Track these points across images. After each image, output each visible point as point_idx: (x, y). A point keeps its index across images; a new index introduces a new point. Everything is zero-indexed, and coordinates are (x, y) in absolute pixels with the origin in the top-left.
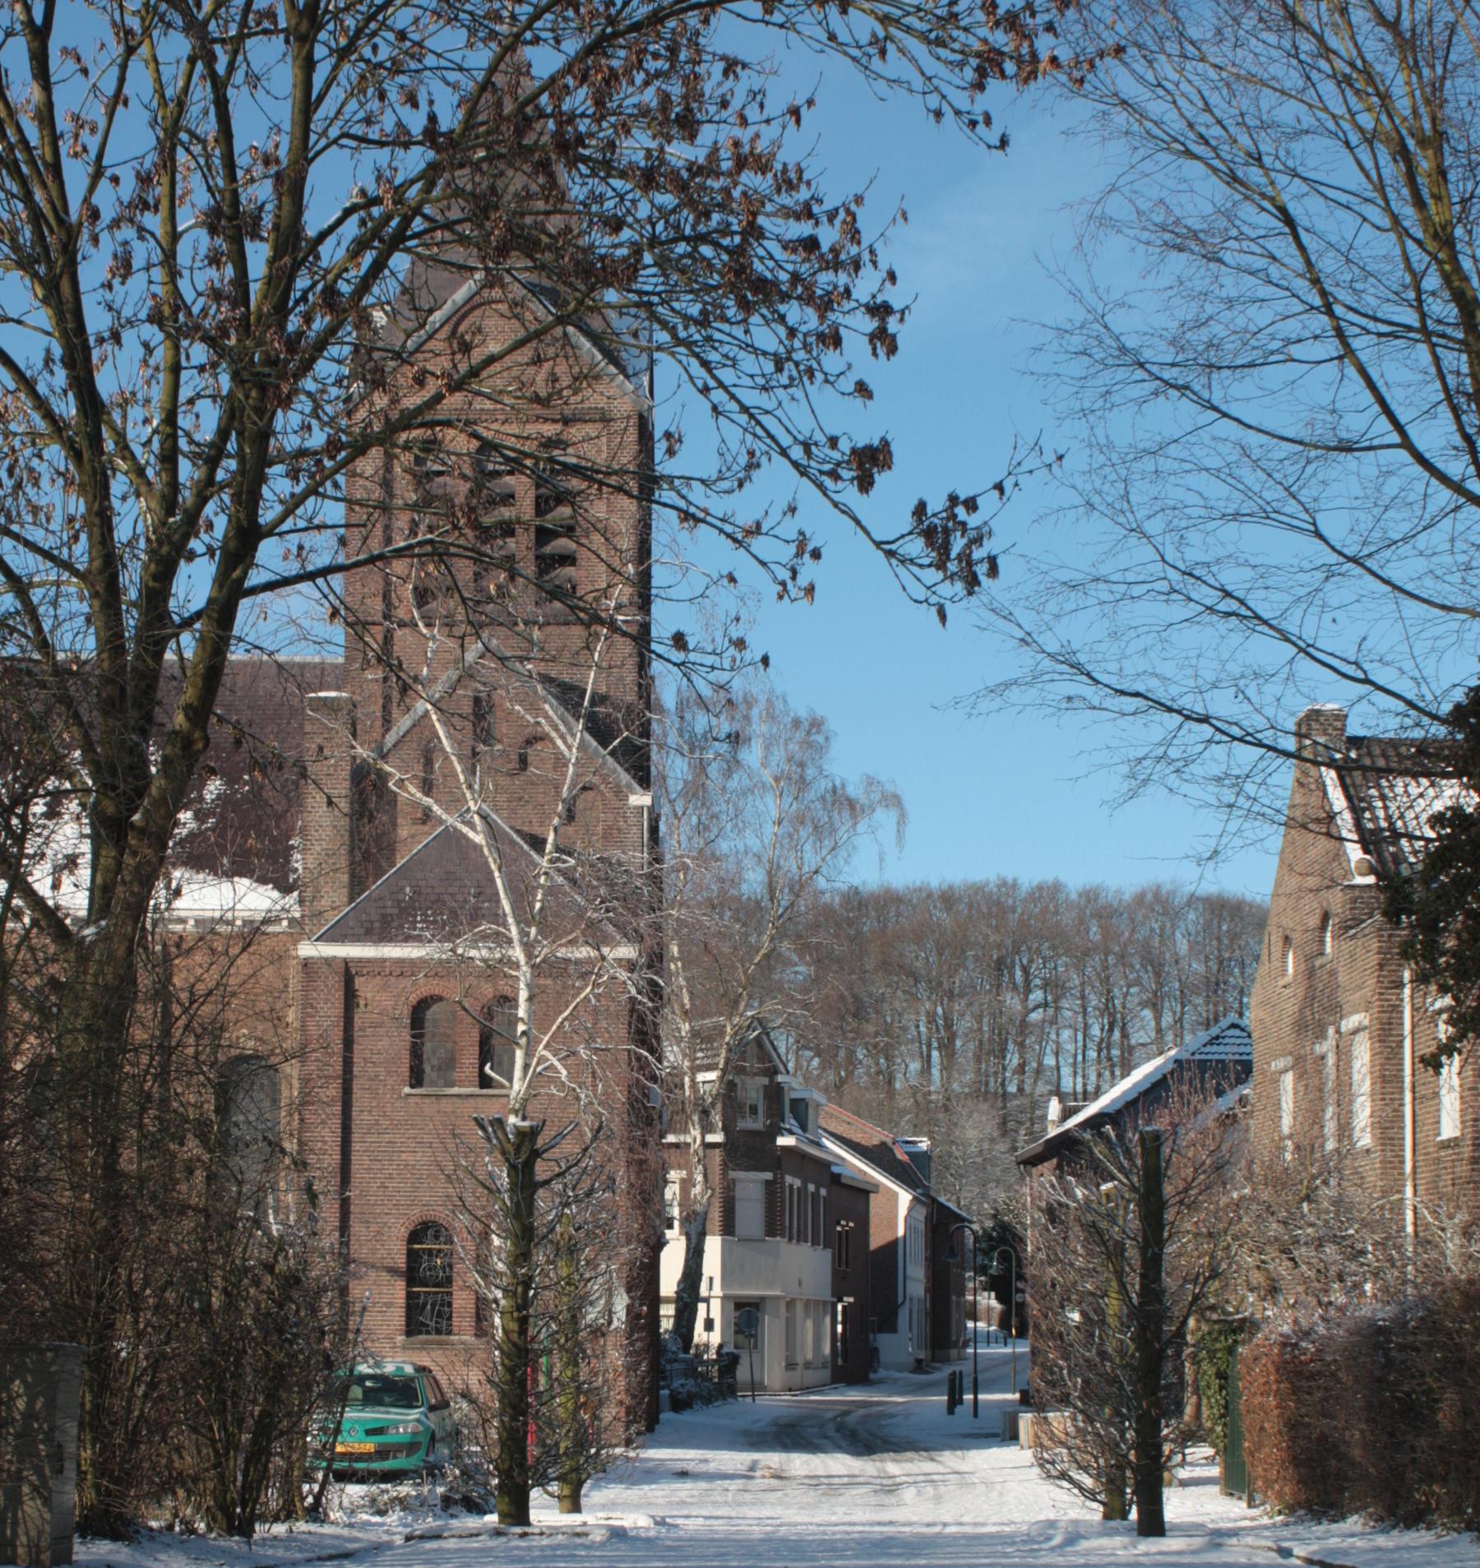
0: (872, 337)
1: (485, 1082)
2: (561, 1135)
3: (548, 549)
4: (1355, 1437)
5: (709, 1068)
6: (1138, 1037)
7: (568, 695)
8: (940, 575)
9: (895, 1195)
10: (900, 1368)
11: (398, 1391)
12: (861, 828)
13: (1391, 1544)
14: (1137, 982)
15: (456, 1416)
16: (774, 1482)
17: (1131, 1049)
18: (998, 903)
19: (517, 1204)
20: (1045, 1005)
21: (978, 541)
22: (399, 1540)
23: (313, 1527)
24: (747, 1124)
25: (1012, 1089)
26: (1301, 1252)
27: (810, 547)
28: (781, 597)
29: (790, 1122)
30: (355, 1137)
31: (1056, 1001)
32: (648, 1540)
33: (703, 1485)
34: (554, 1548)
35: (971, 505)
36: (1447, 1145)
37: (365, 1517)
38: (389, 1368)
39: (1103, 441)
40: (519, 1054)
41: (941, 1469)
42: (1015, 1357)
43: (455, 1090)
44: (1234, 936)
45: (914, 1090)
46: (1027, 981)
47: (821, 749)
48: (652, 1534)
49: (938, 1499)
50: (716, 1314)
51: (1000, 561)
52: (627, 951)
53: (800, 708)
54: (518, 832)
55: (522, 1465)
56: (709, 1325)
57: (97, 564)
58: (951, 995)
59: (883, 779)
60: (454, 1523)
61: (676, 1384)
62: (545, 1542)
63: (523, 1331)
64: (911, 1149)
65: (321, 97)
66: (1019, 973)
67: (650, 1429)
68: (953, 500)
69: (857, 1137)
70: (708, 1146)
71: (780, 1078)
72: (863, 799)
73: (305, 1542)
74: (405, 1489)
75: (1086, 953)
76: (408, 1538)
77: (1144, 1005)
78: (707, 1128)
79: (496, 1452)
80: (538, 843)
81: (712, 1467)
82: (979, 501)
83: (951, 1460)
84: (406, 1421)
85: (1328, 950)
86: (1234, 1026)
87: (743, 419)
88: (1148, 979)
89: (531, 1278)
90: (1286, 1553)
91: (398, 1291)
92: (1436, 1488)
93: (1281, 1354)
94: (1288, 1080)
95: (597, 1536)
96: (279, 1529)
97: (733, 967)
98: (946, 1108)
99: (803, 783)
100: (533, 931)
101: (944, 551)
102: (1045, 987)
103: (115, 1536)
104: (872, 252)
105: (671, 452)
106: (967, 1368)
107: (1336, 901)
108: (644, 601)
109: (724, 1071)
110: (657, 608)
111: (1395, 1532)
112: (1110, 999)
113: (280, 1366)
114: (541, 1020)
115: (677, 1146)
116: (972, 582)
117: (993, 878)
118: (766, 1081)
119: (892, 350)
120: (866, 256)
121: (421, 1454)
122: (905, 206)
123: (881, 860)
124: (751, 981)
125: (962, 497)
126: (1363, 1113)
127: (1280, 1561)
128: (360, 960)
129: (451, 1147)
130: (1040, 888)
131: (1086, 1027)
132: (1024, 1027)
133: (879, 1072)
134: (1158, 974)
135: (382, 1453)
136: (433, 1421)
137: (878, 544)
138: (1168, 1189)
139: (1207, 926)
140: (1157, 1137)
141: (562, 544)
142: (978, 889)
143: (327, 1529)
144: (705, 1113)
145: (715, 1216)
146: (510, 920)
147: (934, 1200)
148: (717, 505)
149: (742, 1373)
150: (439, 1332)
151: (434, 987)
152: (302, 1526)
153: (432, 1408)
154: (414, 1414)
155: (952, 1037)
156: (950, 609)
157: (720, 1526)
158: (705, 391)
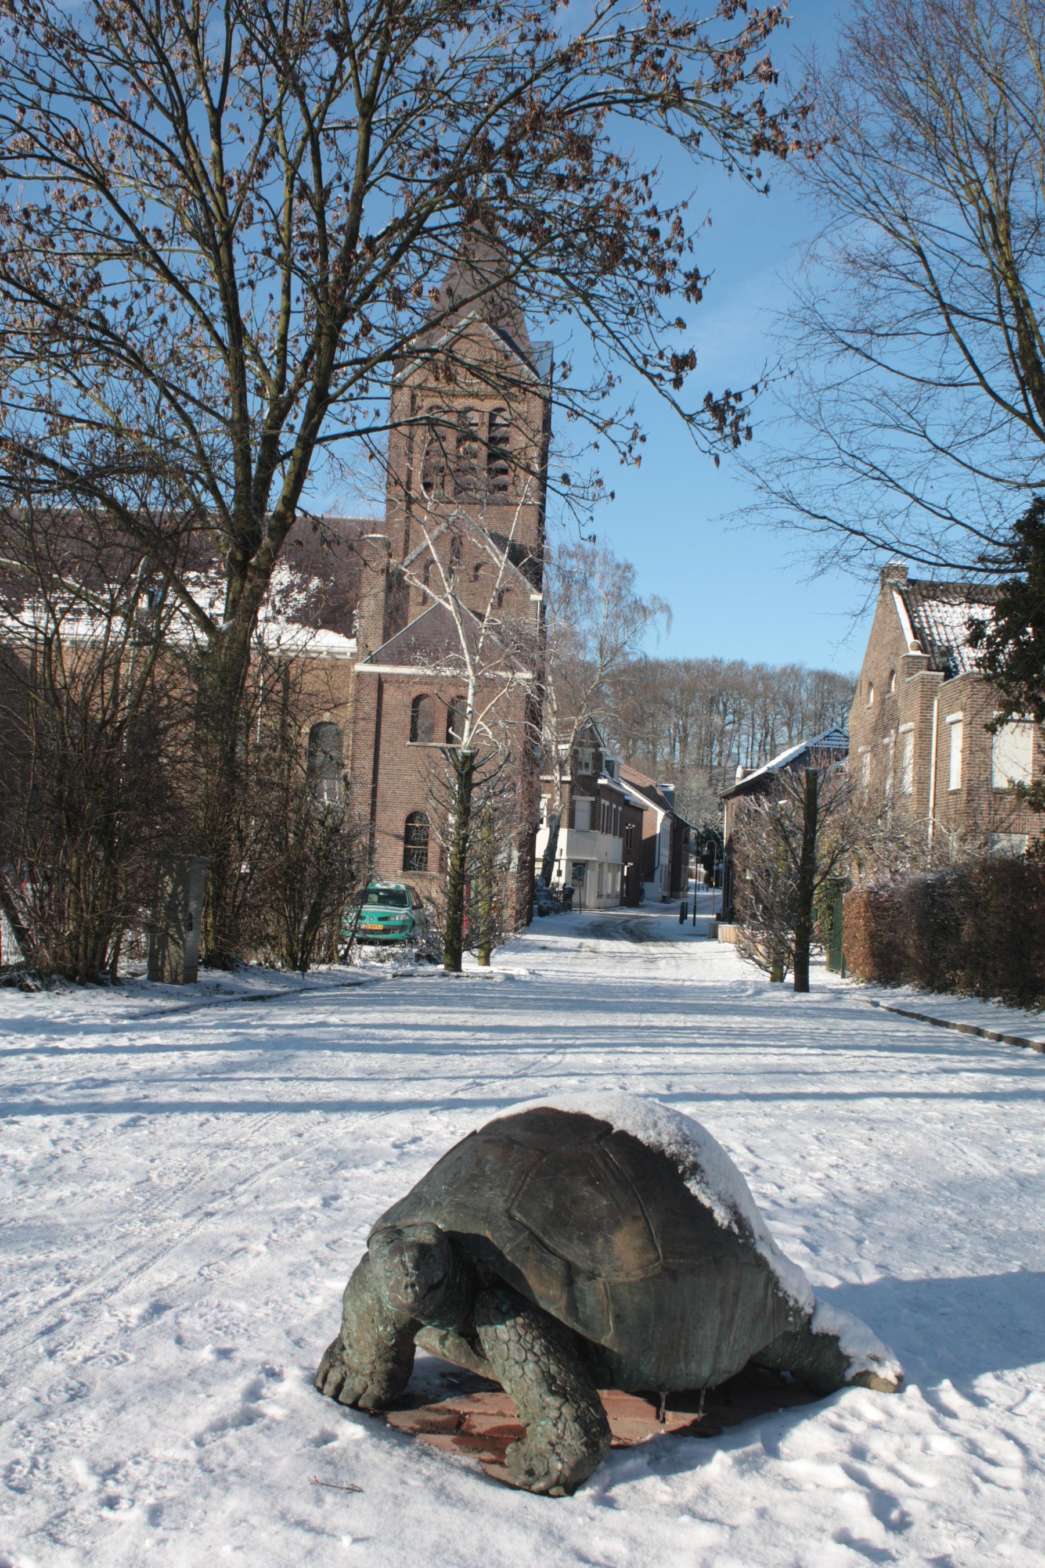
0: (688, 290)
1: (449, 739)
2: (486, 759)
3: (493, 466)
4: (911, 943)
5: (565, 742)
6: (779, 740)
7: (500, 540)
8: (719, 435)
9: (656, 812)
11: (395, 898)
12: (649, 621)
13: (934, 1002)
14: (780, 713)
17: (776, 746)
18: (713, 671)
20: (734, 722)
21: (741, 417)
22: (389, 977)
23: (343, 968)
24: (583, 772)
25: (715, 763)
26: (875, 845)
29: (605, 772)
30: (381, 766)
32: (526, 982)
33: (554, 954)
34: (474, 984)
35: (738, 397)
36: (955, 793)
39: (807, 379)
40: (467, 723)
42: (714, 897)
44: (830, 692)
45: (667, 762)
46: (725, 710)
47: (630, 581)
49: (677, 967)
50: (563, 868)
52: (528, 675)
53: (620, 558)
54: (474, 612)
55: (459, 939)
56: (559, 873)
57: (237, 415)
58: (687, 715)
60: (421, 968)
61: (542, 902)
62: (469, 981)
63: (462, 865)
65: (373, 166)
66: (721, 707)
67: (528, 924)
68: (728, 394)
69: (638, 782)
70: (563, 782)
74: (396, 949)
75: (756, 697)
76: (394, 976)
77: (783, 724)
78: (563, 773)
79: (444, 931)
80: (481, 617)
81: (559, 945)
82: (743, 395)
83: (683, 947)
84: (400, 914)
87: (611, 342)
90: (876, 1004)
91: (399, 848)
94: (867, 759)
95: (498, 979)
96: (323, 968)
98: (682, 772)
99: (620, 597)
101: (723, 420)
102: (734, 712)
103: (225, 968)
105: (565, 376)
106: (690, 901)
107: (899, 664)
108: (544, 459)
110: (552, 461)
112: (766, 721)
113: (325, 877)
114: (479, 705)
115: (547, 782)
116: (737, 442)
117: (710, 657)
119: (699, 298)
120: (686, 244)
121: (407, 931)
124: (588, 699)
125: (733, 392)
126: (909, 778)
132: (722, 732)
134: (791, 709)
135: (386, 931)
136: (414, 914)
137: (683, 415)
138: (820, 802)
139: (817, 686)
140: (815, 774)
141: (501, 463)
142: (702, 663)
143: (350, 969)
145: (565, 818)
148: (589, 406)
149: (575, 898)
150: (420, 869)
151: (425, 689)
152: (337, 967)
153: (414, 908)
154: (404, 910)
155: (686, 736)
156: (723, 457)
157: (564, 976)
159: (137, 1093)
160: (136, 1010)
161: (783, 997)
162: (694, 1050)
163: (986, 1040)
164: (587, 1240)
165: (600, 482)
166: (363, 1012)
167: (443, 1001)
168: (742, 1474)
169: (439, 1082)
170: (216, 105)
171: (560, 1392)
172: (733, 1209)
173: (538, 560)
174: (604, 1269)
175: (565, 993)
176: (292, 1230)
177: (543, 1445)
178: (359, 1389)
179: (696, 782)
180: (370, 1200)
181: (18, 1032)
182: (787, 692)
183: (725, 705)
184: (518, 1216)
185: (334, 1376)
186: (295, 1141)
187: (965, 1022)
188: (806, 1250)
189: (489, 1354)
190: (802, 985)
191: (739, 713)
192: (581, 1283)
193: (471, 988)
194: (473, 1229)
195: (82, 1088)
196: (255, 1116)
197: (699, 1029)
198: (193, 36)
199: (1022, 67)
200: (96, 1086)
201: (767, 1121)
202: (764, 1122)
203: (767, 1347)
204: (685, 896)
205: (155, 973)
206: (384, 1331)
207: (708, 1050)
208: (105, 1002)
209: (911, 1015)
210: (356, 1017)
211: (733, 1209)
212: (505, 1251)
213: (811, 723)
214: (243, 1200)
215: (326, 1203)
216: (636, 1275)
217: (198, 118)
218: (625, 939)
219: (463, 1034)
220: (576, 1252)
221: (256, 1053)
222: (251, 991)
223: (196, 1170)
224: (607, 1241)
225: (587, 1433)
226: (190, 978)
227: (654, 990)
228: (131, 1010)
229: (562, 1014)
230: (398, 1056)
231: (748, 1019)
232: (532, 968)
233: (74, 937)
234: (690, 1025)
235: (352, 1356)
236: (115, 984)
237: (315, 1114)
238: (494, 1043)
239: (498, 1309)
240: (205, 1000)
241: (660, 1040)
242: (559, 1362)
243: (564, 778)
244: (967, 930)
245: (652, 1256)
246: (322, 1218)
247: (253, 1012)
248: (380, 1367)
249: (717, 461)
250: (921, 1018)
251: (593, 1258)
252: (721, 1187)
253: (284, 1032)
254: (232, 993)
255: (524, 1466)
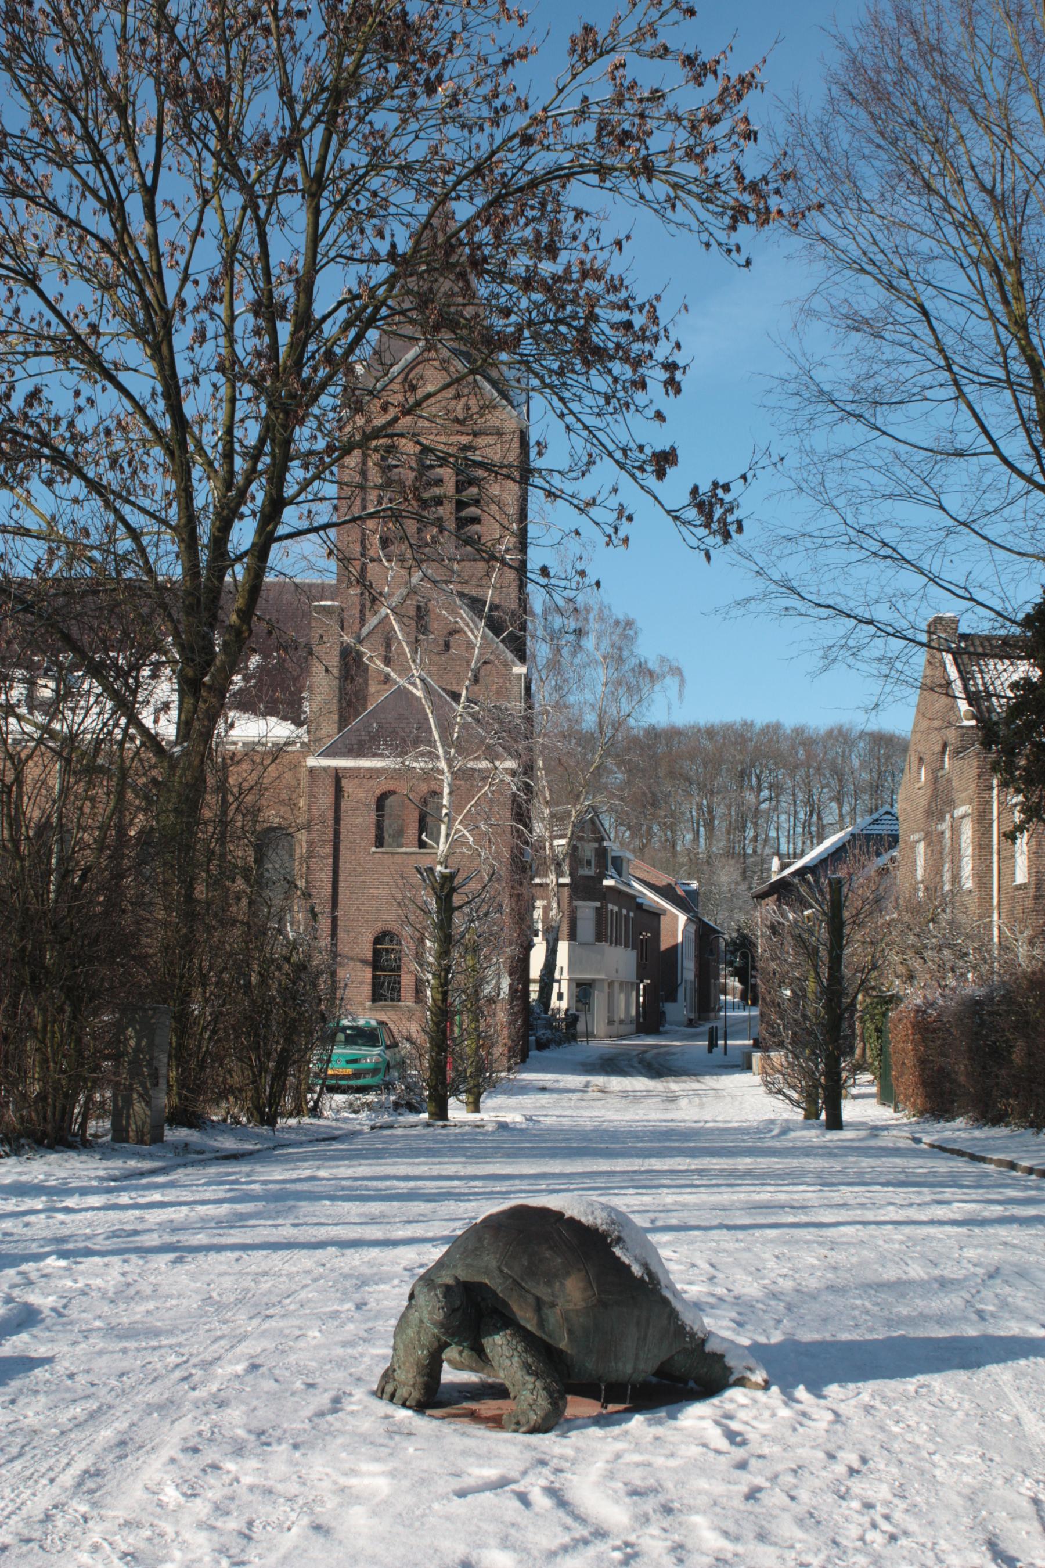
0: (666, 383)
1: (422, 845)
3: (463, 514)
4: (961, 1069)
5: (561, 837)
7: (475, 604)
8: (707, 531)
9: (676, 917)
10: (679, 1024)
11: (366, 1037)
12: (657, 688)
14: (828, 785)
15: (403, 1052)
16: (600, 1094)
17: (823, 827)
18: (742, 736)
19: (442, 921)
20: (770, 799)
21: (730, 510)
22: (367, 1129)
23: (313, 1121)
24: (585, 872)
25: (750, 851)
27: (626, 514)
28: (608, 545)
29: (612, 871)
30: (341, 878)
31: (777, 796)
32: (521, 1130)
33: (556, 1096)
35: (726, 488)
36: (1019, 888)
37: (346, 1114)
38: (361, 1022)
40: (443, 828)
41: (704, 1087)
43: (404, 850)
44: (888, 757)
45: (689, 852)
46: (759, 784)
47: (632, 639)
48: (524, 1126)
49: (702, 1105)
50: (565, 990)
51: (744, 523)
52: (511, 764)
53: (619, 614)
54: (444, 689)
56: (560, 997)
58: (712, 792)
59: (671, 658)
60: (401, 1118)
61: (540, 1033)
64: (687, 888)
65: (324, 232)
66: (754, 779)
67: (523, 1061)
68: (715, 485)
69: (653, 880)
71: (605, 844)
72: (658, 671)
73: (308, 1130)
74: (371, 1097)
75: (796, 767)
76: (372, 1128)
77: (831, 799)
78: (560, 874)
80: (456, 697)
81: (561, 1085)
82: (732, 486)
84: (371, 1055)
85: (947, 766)
86: (888, 813)
87: (585, 433)
88: (834, 783)
89: (450, 967)
90: (918, 1141)
91: (367, 974)
92: (1011, 1101)
93: (915, 1017)
94: (921, 847)
95: (490, 1128)
96: (292, 1122)
97: (577, 774)
98: (708, 863)
99: (621, 660)
100: (453, 751)
101: (709, 516)
103: (190, 1126)
104: (666, 330)
105: (540, 454)
106: (720, 1024)
107: (951, 735)
108: (523, 546)
109: (571, 839)
110: (531, 551)
111: (986, 1128)
112: (810, 796)
113: (294, 1020)
114: (457, 806)
115: (541, 885)
116: (727, 536)
118: (596, 845)
119: (678, 391)
120: (662, 333)
121: (381, 1076)
122: (686, 302)
123: (669, 708)
124: (587, 784)
127: (914, 1145)
128: (345, 769)
129: (401, 885)
130: (768, 726)
131: (796, 813)
132: (757, 813)
133: (667, 840)
134: (840, 780)
135: (357, 1075)
136: (388, 1055)
137: (669, 512)
138: (846, 914)
139: (871, 751)
142: (728, 727)
143: (322, 1122)
144: (559, 865)
145: (565, 929)
146: (438, 744)
147: (700, 920)
148: (569, 487)
149: (581, 1027)
150: (392, 1000)
151: (391, 785)
152: (306, 1120)
153: (388, 1047)
154: (377, 1051)
155: (712, 819)
158: (562, 416)
159: (168, 1239)
160: (117, 1173)
161: (815, 1136)
162: (689, 1190)
163: (1019, 1174)
164: (549, 1283)
165: (582, 573)
166: (350, 1166)
167: (430, 1153)
168: (650, 1425)
169: (437, 1223)
170: (149, 182)
171: (536, 1375)
172: (646, 1266)
173: (520, 634)
174: (560, 1302)
175: (564, 1140)
176: (336, 1323)
177: (525, 1407)
178: (406, 1395)
179: (727, 876)
180: (393, 1304)
181: (16, 1196)
182: (834, 760)
183: (758, 777)
184: (505, 1270)
185: (389, 1389)
186: (321, 1269)
187: (1002, 1156)
188: (734, 1325)
189: (490, 1355)
190: (835, 1122)
191: (776, 788)
192: (546, 1311)
193: (461, 1138)
194: (477, 1279)
195: (118, 1237)
196: (280, 1253)
197: (700, 1172)
198: (122, 107)
199: (1025, 109)
200: (129, 1236)
201: (737, 1245)
202: (732, 1246)
203: (672, 1357)
204: (717, 1018)
205: (120, 1134)
206: (421, 1353)
207: (703, 1189)
208: (78, 1165)
209: (952, 1151)
210: (344, 1170)
211: (646, 1266)
212: (499, 1291)
213: (866, 797)
214: (292, 1307)
215: (358, 1307)
216: (581, 1305)
217: (134, 206)
218: (641, 1074)
219: (456, 1183)
220: (542, 1291)
221: (260, 1205)
222: (226, 1149)
223: (247, 1290)
224: (562, 1284)
225: (551, 1397)
226: (157, 1138)
227: (667, 1134)
228: (111, 1172)
229: (558, 1161)
230: (395, 1203)
231: (759, 1160)
232: (528, 1113)
233: (42, 1097)
234: (693, 1167)
235: (400, 1375)
236: (85, 1147)
237: (332, 1250)
238: (488, 1190)
239: (495, 1325)
240: (179, 1160)
241: (656, 1182)
242: (533, 1356)
243: (562, 881)
244: (1018, 1056)
245: (590, 1293)
246: (357, 1315)
247: (237, 1169)
248: (420, 1380)
249: (708, 557)
250: (960, 1153)
251: (553, 1295)
252: (637, 1252)
253: (278, 1186)
254: (202, 1152)
255: (514, 1420)
